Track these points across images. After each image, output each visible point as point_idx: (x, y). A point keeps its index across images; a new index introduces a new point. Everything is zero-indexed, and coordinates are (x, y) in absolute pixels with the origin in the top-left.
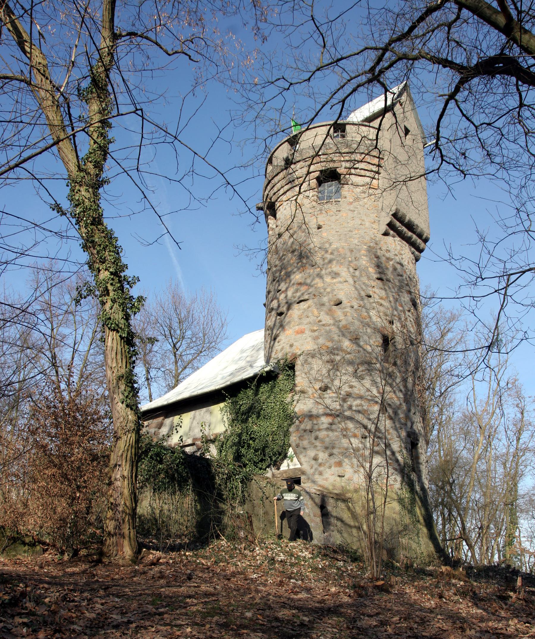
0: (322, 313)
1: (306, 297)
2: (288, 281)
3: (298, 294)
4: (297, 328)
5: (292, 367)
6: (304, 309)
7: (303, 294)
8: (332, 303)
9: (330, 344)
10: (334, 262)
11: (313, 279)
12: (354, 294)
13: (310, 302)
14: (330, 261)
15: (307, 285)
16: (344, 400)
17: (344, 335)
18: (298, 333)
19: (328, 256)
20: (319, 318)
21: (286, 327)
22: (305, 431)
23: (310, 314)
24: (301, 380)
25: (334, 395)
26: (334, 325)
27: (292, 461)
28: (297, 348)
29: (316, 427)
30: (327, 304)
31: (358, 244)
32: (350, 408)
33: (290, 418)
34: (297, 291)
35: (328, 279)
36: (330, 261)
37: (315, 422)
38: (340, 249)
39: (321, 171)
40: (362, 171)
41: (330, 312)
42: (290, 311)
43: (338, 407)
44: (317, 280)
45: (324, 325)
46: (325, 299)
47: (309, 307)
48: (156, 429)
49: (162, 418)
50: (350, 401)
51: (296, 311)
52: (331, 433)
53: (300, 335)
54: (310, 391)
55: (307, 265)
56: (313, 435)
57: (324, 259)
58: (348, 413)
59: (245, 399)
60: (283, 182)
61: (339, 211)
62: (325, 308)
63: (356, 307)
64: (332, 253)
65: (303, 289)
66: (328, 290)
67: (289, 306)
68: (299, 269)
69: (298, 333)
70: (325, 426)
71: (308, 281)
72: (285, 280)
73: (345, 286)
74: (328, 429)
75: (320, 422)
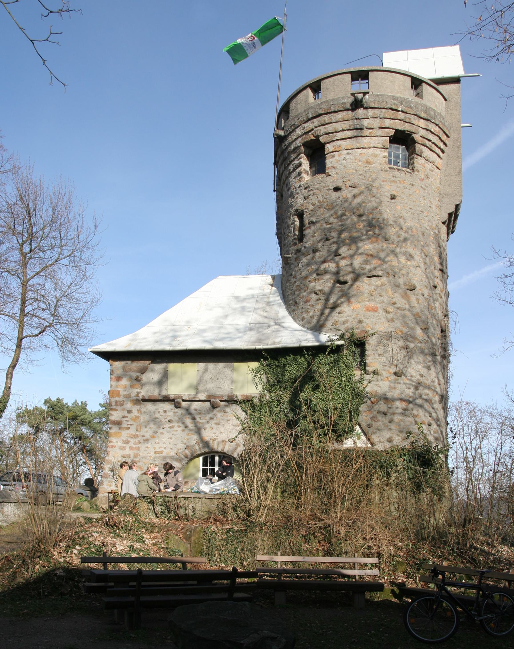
0: (397, 295)
1: (380, 273)
2: (354, 247)
3: (368, 267)
4: (367, 304)
5: (360, 345)
6: (377, 286)
7: (375, 268)
8: (407, 287)
9: (405, 330)
10: (409, 242)
11: (387, 255)
12: (425, 281)
13: (384, 279)
14: (405, 240)
15: (380, 259)
16: (416, 388)
17: (417, 323)
18: (368, 309)
19: (403, 235)
20: (394, 300)
21: (352, 300)
22: (379, 412)
23: (384, 293)
24: (373, 361)
25: (408, 382)
26: (409, 310)
27: (359, 439)
28: (368, 326)
29: (391, 411)
30: (402, 286)
31: (428, 228)
32: (420, 396)
33: (359, 396)
34: (366, 262)
35: (403, 259)
36: (405, 240)
37: (390, 406)
38: (414, 229)
39: (397, 131)
40: (433, 145)
41: (405, 296)
42: (357, 283)
43: (411, 394)
44: (391, 257)
45: (398, 308)
46: (401, 281)
47: (382, 285)
48: (138, 374)
49: (148, 362)
50: (421, 390)
51: (365, 285)
52: (406, 419)
53: (371, 313)
54: (385, 374)
55: (380, 237)
56: (388, 417)
57: (399, 237)
58: (419, 401)
59: (295, 368)
60: (346, 125)
61: (413, 185)
62: (401, 291)
63: (426, 296)
64: (406, 232)
65: (375, 262)
66: (404, 272)
67: (357, 277)
68: (369, 238)
69: (368, 309)
70: (400, 411)
71: (382, 255)
72: (349, 245)
73: (418, 271)
74: (403, 414)
75: (395, 406)
